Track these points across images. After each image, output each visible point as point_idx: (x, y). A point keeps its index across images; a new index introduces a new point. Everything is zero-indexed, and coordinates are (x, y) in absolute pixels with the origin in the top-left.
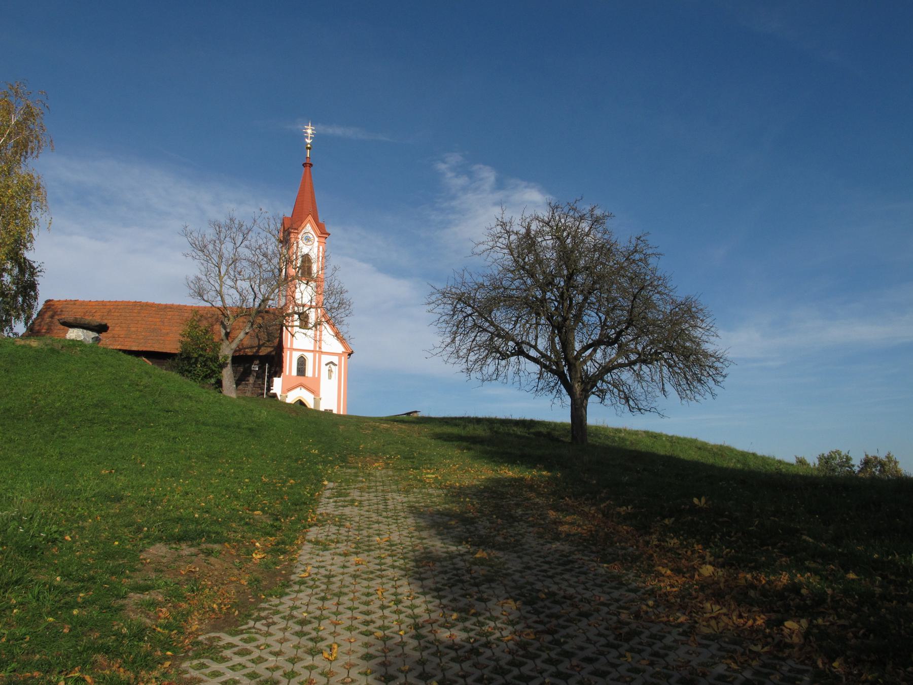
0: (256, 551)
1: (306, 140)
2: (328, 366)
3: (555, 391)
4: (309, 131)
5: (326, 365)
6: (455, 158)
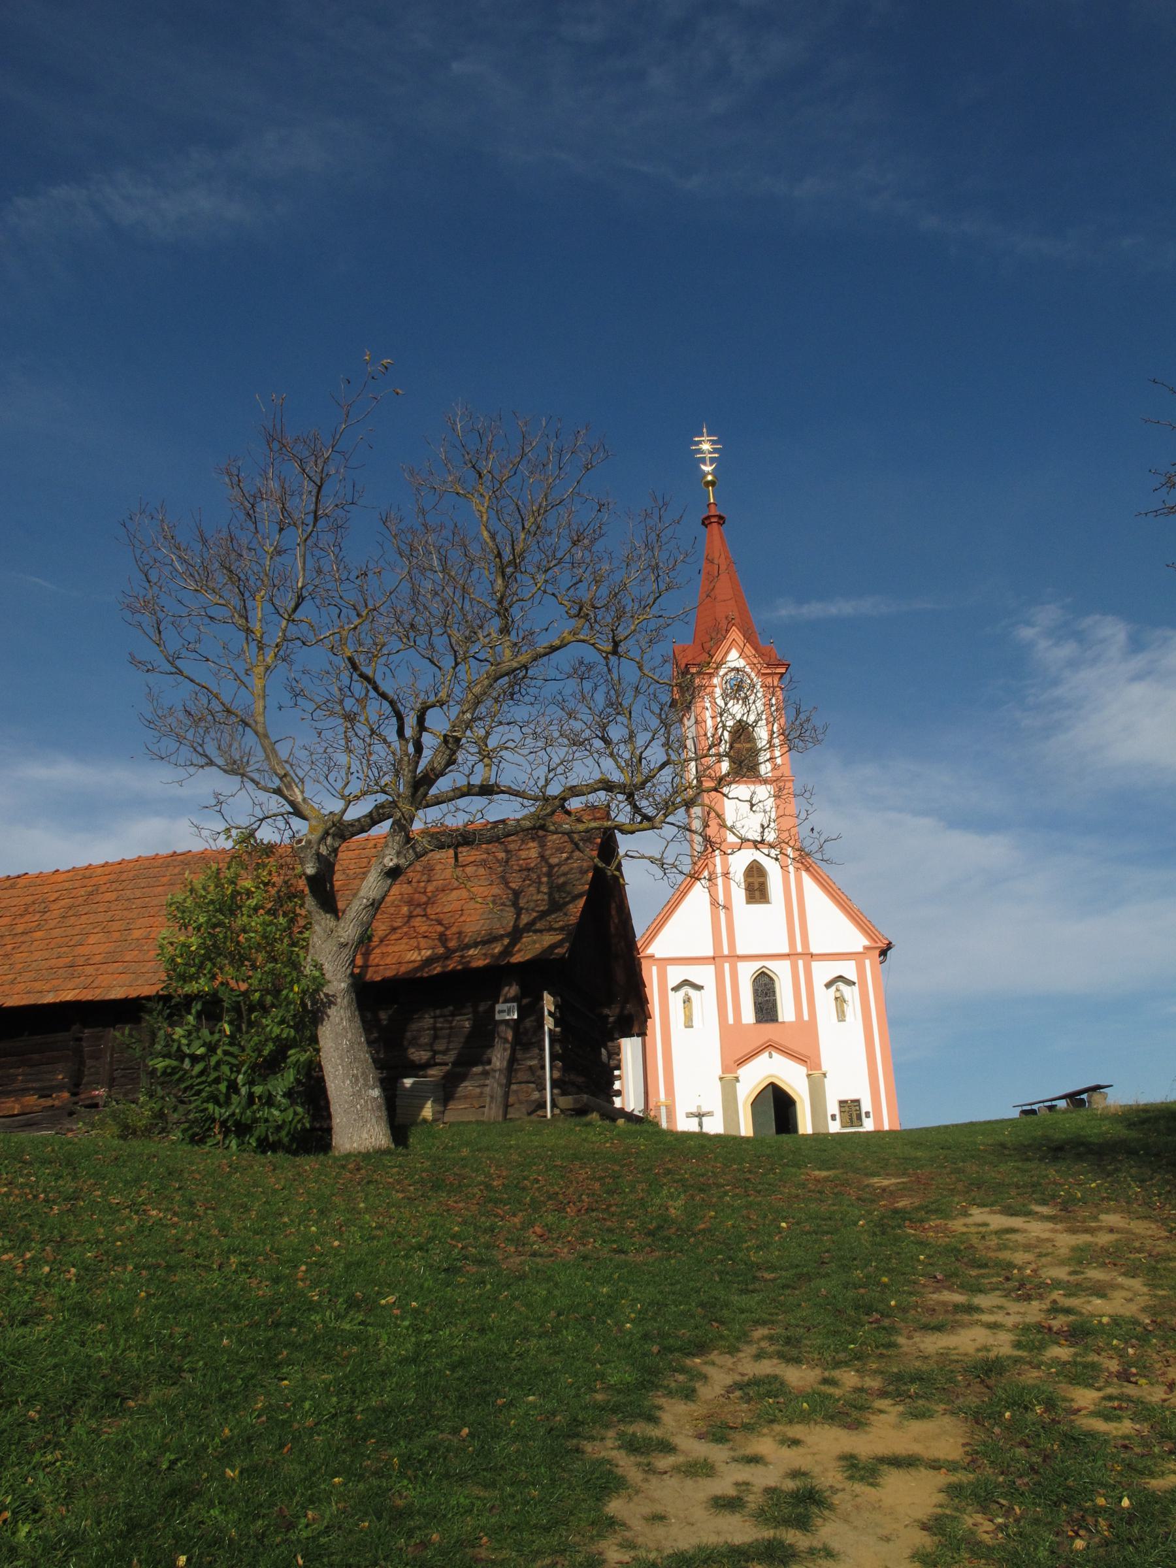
1: (703, 467)
2: (833, 988)
4: (706, 447)
6: (1048, 614)
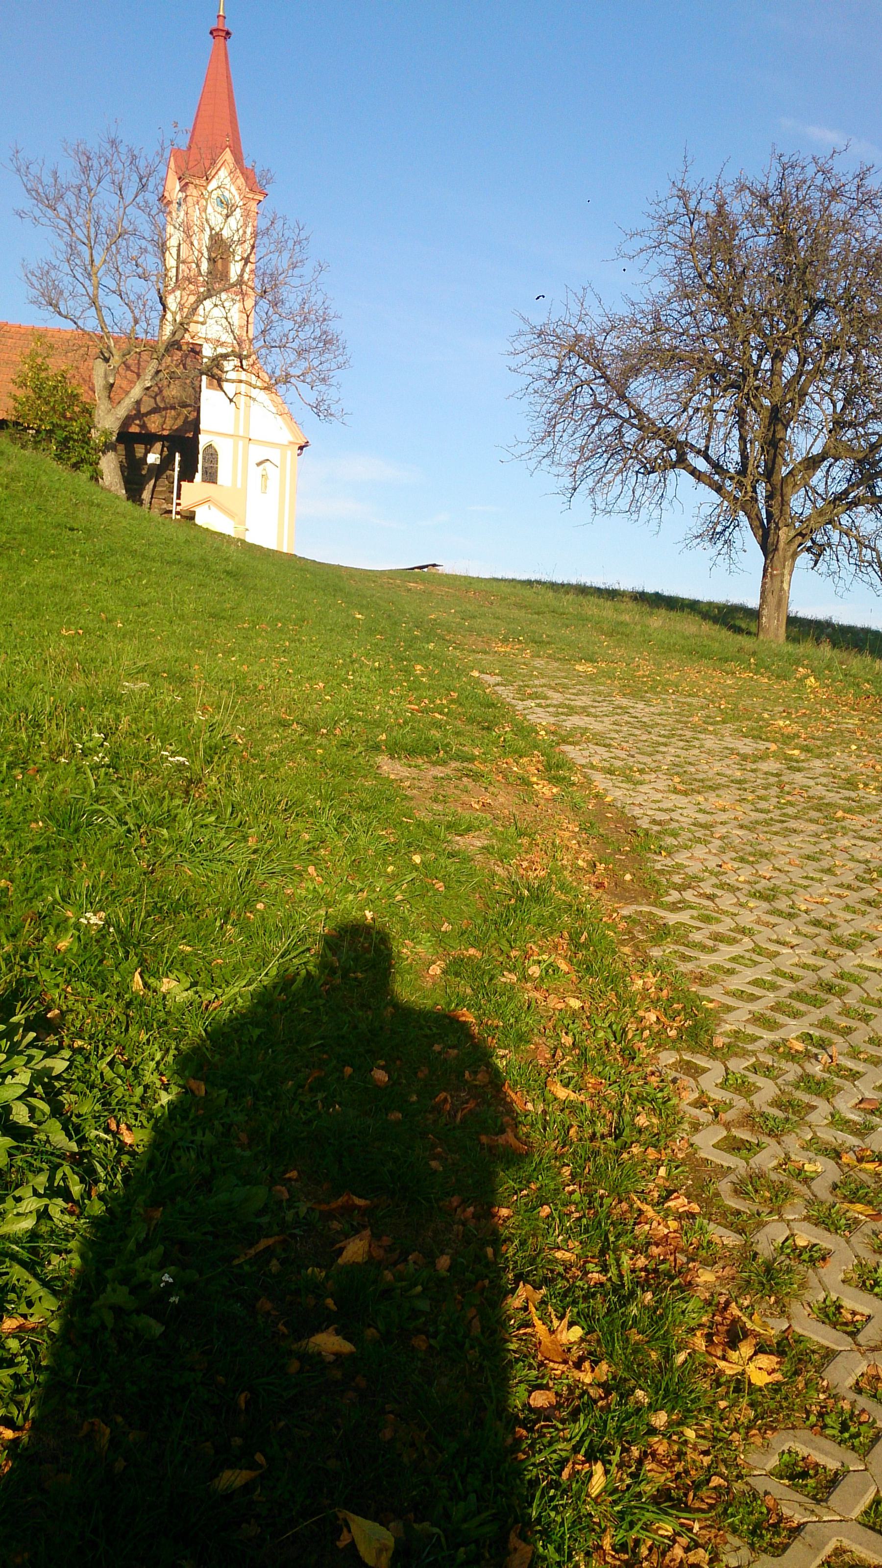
0: (828, 682)
2: (262, 467)
3: (721, 542)
5: (259, 464)
